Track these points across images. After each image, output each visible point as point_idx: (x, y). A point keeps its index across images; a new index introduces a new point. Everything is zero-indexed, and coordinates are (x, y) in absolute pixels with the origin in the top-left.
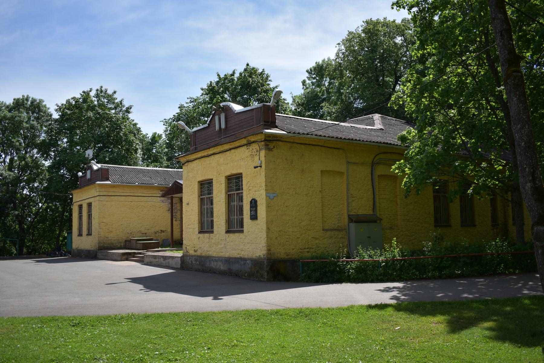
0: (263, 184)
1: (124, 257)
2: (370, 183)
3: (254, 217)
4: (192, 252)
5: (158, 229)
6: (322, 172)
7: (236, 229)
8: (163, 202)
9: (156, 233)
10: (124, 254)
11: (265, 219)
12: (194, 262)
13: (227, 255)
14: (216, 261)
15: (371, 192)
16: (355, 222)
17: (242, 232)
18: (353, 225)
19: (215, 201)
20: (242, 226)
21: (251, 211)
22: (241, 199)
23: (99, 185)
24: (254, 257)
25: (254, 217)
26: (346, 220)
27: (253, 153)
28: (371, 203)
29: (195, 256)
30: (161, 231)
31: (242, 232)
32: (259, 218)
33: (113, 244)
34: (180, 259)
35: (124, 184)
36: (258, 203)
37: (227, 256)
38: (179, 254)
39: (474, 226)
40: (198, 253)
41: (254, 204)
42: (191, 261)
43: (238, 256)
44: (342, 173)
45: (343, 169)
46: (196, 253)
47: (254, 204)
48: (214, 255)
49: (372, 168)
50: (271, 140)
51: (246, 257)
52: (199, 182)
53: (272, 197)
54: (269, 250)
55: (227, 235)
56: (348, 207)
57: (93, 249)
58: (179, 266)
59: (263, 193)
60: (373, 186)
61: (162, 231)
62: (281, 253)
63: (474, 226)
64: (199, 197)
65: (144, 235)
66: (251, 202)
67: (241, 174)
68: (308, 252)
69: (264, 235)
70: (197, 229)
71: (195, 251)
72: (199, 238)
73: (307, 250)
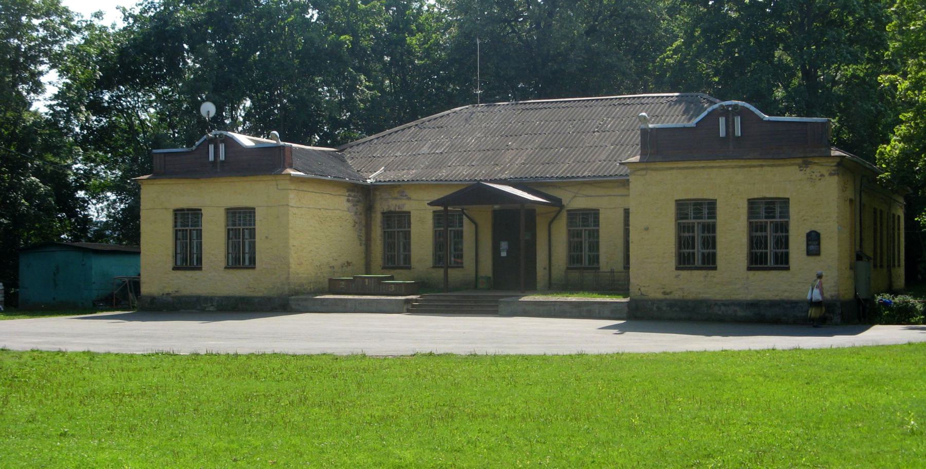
13: (750, 297)
14: (724, 305)
21: (808, 245)
27: (814, 177)
29: (666, 300)
36: (822, 236)
40: (677, 295)
41: (813, 239)
42: (658, 308)
43: (777, 298)
46: (668, 297)
47: (813, 239)
48: (718, 297)
51: (794, 298)
55: (752, 273)
57: (260, 294)
61: (349, 264)
71: (664, 293)
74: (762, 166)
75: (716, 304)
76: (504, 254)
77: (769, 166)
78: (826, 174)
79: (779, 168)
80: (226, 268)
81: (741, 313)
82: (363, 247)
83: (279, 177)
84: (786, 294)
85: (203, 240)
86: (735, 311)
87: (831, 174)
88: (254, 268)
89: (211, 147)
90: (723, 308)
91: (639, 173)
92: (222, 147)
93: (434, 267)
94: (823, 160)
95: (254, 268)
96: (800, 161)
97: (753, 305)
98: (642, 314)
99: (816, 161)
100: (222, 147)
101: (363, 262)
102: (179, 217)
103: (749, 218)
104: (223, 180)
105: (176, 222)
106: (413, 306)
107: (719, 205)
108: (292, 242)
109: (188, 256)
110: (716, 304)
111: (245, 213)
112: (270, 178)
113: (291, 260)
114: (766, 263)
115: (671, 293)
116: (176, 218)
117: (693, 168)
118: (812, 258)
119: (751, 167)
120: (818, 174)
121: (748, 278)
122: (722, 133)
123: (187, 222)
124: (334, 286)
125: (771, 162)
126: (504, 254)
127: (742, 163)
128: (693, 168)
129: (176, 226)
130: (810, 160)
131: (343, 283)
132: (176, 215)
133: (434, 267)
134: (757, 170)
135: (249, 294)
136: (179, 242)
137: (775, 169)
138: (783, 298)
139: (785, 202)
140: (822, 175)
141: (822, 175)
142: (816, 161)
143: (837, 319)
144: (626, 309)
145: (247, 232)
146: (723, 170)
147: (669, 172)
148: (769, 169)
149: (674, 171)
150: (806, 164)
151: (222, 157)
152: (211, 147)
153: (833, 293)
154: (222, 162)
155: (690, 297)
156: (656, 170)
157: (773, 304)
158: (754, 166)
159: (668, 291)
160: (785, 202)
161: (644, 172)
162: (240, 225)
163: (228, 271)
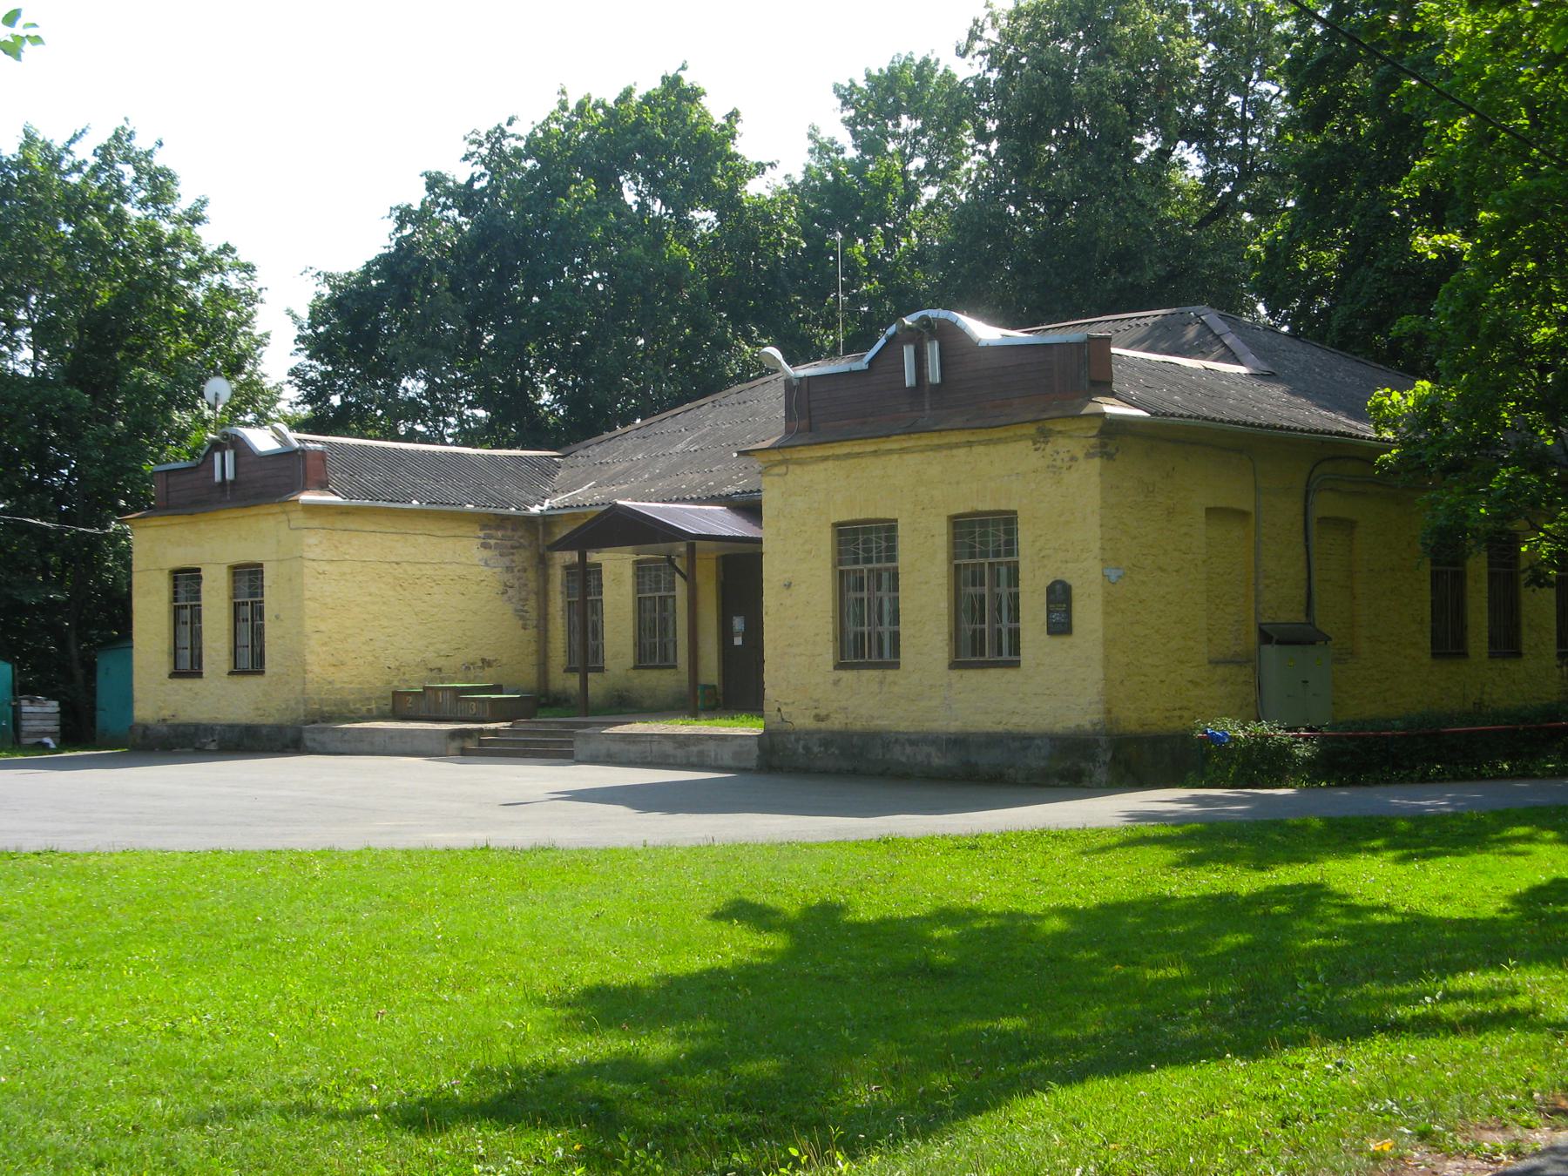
0: (1096, 546)
1: (456, 744)
2: (1301, 539)
3: (1060, 626)
4: (804, 721)
5: (472, 655)
6: (1210, 511)
7: (986, 658)
8: (487, 564)
9: (468, 668)
10: (454, 735)
11: (1100, 634)
12: (816, 749)
13: (954, 726)
14: (912, 743)
15: (1302, 564)
16: (1279, 642)
17: (1015, 664)
18: (1271, 651)
19: (903, 582)
20: (1015, 648)
21: (1049, 612)
22: (1014, 578)
23: (311, 508)
24: (1058, 728)
25: (1060, 626)
26: (1254, 637)
27: (1059, 463)
28: (1303, 592)
29: (819, 731)
30: (483, 660)
31: (1015, 664)
32: (1075, 630)
33: (346, 703)
34: (754, 743)
35: (447, 508)
36: (1075, 592)
37: (901, 729)
38: (746, 728)
39: (1518, 654)
40: (836, 723)
41: (1060, 597)
42: (806, 748)
43: (1000, 728)
44: (1243, 515)
45: (1247, 506)
46: (823, 725)
47: (1060, 597)
48: (903, 726)
49: (1306, 500)
50: (1113, 429)
51: (1029, 729)
52: (836, 525)
53: (1113, 578)
54: (1109, 711)
55: (956, 674)
56: (1257, 602)
57: (270, 721)
58: (753, 763)
59: (1094, 568)
60: (1307, 547)
61: (486, 663)
62: (1131, 718)
63: (1518, 654)
64: (834, 566)
65: (434, 674)
66: (1051, 590)
67: (1015, 512)
68: (1181, 717)
69: (1098, 674)
70: (830, 657)
71: (818, 718)
72: (836, 683)
73: (1177, 713)
74: (970, 444)
75: (897, 741)
76: (738, 641)
77: (980, 443)
78: (1080, 455)
79: (1001, 447)
80: (231, 673)
81: (937, 761)
82: (532, 632)
83: (289, 507)
84: (1016, 719)
85: (901, 594)
86: (929, 755)
87: (1089, 456)
88: (262, 673)
89: (908, 352)
90: (908, 750)
91: (776, 470)
92: (933, 350)
93: (635, 668)
94: (1071, 425)
95: (262, 673)
96: (1031, 430)
97: (958, 742)
98: (808, 767)
99: (1059, 427)
100: (933, 350)
101: (533, 659)
102: (182, 583)
103: (839, 560)
104: (223, 515)
105: (175, 593)
106: (481, 743)
107: (901, 531)
108: (309, 625)
109: (865, 641)
110: (897, 741)
111: (865, 531)
112: (276, 509)
113: (310, 658)
114: (983, 654)
115: (828, 716)
116: (175, 586)
117: (858, 455)
118: (1057, 641)
119: (951, 446)
120: (1066, 457)
121: (950, 685)
122: (909, 379)
123: (864, 549)
124: (401, 705)
125: (983, 435)
126: (738, 641)
127: (935, 439)
128: (858, 455)
129: (176, 600)
130: (1049, 425)
131: (410, 698)
132: (175, 579)
133: (635, 668)
134: (962, 452)
135: (258, 720)
136: (241, 625)
137: (992, 449)
138: (1010, 727)
139: (1008, 521)
140: (1073, 459)
141: (1073, 459)
142: (1059, 427)
143: (1101, 775)
144: (756, 752)
145: (885, 576)
146: (907, 457)
147: (822, 466)
148: (981, 449)
149: (830, 464)
150: (1045, 435)
151: (934, 375)
152: (908, 352)
153: (1096, 717)
154: (935, 387)
155: (858, 726)
156: (800, 463)
157: (993, 740)
158: (957, 446)
159: (823, 712)
160: (1008, 521)
161: (783, 469)
162: (985, 554)
163: (236, 678)
